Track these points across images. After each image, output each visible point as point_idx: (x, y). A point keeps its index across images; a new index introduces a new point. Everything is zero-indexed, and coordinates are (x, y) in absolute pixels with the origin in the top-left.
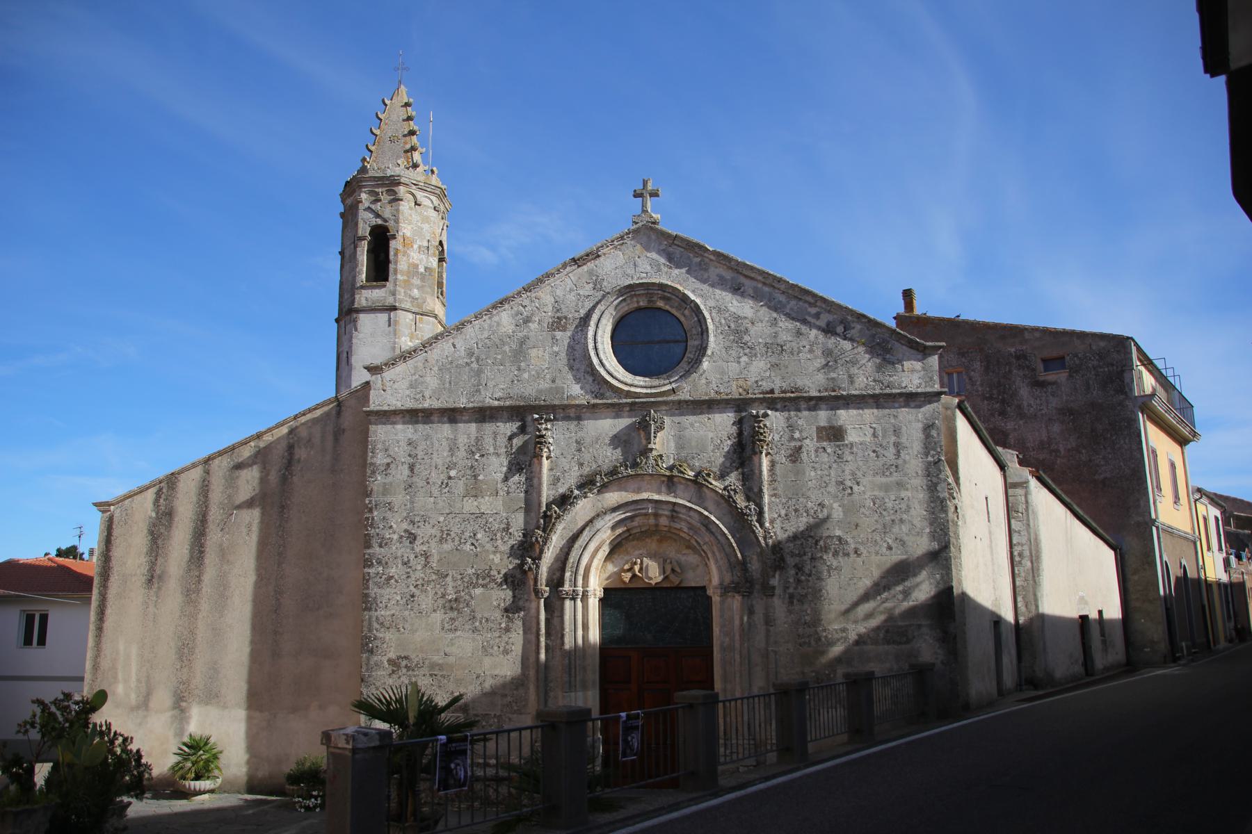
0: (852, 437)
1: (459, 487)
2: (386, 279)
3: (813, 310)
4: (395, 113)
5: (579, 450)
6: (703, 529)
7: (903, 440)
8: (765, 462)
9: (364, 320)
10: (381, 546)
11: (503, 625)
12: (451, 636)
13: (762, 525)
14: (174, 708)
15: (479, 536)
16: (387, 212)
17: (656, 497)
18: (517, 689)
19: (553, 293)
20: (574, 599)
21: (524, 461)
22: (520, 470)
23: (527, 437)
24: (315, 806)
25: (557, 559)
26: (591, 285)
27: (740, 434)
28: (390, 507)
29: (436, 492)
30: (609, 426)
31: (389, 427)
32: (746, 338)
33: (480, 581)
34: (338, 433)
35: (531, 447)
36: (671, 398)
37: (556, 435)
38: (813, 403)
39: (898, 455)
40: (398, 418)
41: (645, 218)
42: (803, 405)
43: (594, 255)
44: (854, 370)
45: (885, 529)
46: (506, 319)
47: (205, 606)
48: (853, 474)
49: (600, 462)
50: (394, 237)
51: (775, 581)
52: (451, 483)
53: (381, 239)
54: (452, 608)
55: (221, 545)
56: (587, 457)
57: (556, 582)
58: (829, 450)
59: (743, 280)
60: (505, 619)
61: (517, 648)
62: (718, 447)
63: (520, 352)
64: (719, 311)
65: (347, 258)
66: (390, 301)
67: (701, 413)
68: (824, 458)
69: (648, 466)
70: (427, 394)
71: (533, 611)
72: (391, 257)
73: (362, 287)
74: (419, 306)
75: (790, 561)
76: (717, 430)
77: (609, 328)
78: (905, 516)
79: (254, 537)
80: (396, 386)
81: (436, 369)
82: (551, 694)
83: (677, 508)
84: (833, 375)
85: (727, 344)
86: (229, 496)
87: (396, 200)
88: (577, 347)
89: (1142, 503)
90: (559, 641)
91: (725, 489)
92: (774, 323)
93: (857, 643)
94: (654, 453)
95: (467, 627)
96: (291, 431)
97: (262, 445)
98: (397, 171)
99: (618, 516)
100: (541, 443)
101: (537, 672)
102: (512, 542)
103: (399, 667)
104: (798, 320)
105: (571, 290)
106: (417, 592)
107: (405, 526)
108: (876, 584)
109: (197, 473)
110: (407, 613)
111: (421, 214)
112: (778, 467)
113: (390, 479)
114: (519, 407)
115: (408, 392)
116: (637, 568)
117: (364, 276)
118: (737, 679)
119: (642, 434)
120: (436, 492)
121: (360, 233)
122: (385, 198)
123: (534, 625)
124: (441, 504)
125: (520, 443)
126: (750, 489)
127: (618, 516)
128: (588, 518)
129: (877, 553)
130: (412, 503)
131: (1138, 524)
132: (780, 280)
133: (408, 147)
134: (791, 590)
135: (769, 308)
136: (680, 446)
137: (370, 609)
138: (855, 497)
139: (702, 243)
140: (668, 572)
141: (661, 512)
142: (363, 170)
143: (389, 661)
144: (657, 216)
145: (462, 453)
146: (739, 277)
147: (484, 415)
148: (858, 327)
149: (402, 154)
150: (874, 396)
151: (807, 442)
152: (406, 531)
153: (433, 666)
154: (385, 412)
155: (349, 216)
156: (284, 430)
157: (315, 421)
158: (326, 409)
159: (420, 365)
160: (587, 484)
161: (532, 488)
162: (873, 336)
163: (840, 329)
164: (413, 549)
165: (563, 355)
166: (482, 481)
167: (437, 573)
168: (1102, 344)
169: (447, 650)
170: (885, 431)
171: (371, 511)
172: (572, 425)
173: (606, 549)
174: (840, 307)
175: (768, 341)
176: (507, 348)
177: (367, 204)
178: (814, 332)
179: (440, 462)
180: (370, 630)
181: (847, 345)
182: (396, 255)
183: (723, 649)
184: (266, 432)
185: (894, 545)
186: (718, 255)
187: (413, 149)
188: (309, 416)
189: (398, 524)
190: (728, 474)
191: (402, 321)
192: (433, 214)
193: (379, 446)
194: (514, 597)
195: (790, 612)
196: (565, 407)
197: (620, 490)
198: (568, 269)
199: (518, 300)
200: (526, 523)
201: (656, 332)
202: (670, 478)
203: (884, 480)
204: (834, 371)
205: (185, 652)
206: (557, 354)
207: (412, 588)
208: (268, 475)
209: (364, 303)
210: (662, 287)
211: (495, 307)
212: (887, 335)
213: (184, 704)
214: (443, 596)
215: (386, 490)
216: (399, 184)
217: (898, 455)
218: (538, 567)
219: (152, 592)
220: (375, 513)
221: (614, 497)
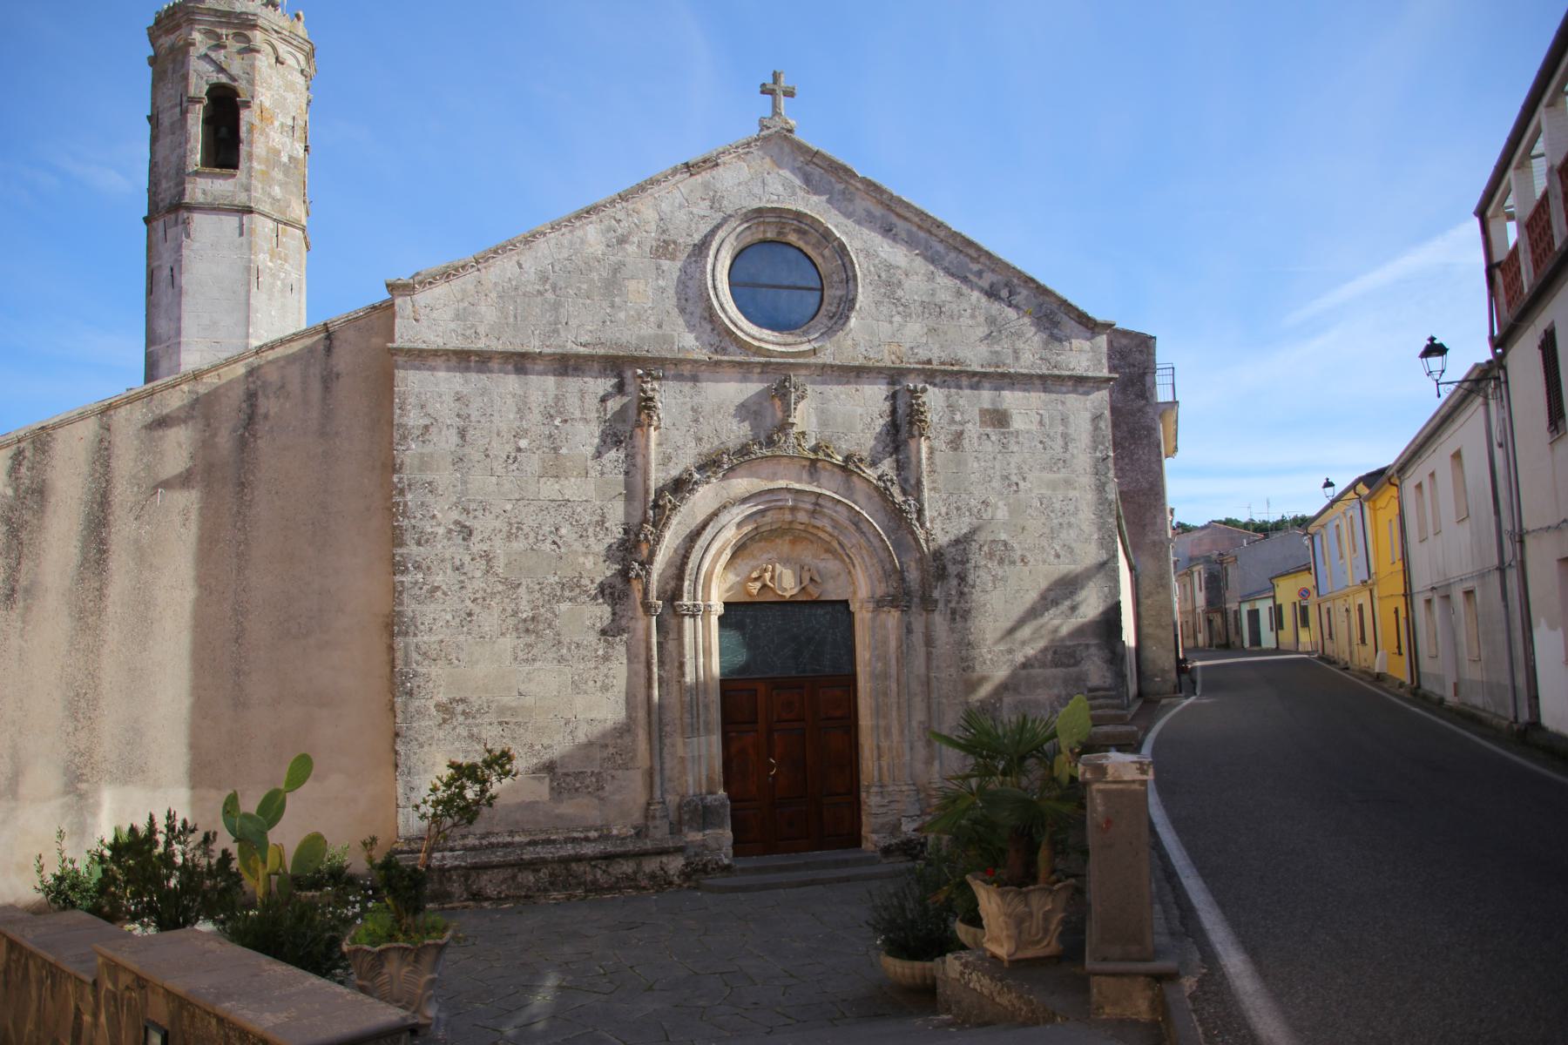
0: (1017, 423)
1: (533, 463)
2: (236, 167)
3: (975, 267)
5: (696, 421)
6: (852, 528)
7: (1071, 431)
8: (924, 445)
10: (419, 544)
11: (600, 652)
12: (527, 668)
13: (922, 525)
14: (66, 793)
15: (563, 531)
16: (236, 66)
17: (797, 486)
18: (621, 737)
19: (656, 207)
20: (694, 616)
21: (623, 431)
22: (618, 443)
23: (626, 399)
24: (356, 916)
25: (669, 564)
26: (708, 203)
27: (894, 412)
28: (431, 487)
29: (499, 470)
30: (733, 391)
32: (900, 293)
33: (567, 593)
34: (329, 380)
35: (632, 412)
36: (812, 360)
37: (668, 398)
38: (976, 379)
39: (1066, 447)
40: (439, 361)
41: (777, 125)
42: (965, 381)
43: (711, 163)
44: (1020, 344)
45: (1053, 534)
46: (592, 235)
47: (113, 634)
48: (1019, 468)
49: (724, 438)
50: (247, 105)
51: (936, 594)
52: (521, 457)
53: (225, 109)
54: (527, 630)
55: (137, 541)
56: (706, 430)
57: (672, 596)
58: (993, 438)
59: (894, 219)
60: (602, 644)
61: (620, 683)
62: (868, 426)
63: (613, 283)
64: (868, 255)
66: (241, 199)
67: (848, 383)
68: (988, 446)
69: (788, 445)
70: (482, 330)
71: (641, 633)
73: (197, 173)
74: (284, 213)
75: (953, 569)
76: (871, 401)
77: (728, 263)
78: (1073, 520)
79: (193, 528)
80: (435, 315)
81: (494, 295)
82: (668, 741)
83: (821, 501)
84: (997, 348)
85: (878, 298)
86: (148, 467)
88: (690, 283)
89: (1159, 521)
90: (676, 672)
91: (880, 478)
92: (931, 277)
93: (1024, 666)
94: (795, 430)
95: (550, 655)
96: (251, 372)
97: (202, 390)
99: (748, 509)
100: (649, 408)
101: (649, 713)
102: (609, 540)
103: (453, 714)
104: (958, 277)
105: (681, 206)
106: (476, 609)
107: (455, 515)
108: (1043, 597)
109: (89, 429)
110: (462, 638)
112: (937, 453)
113: (428, 449)
114: (617, 357)
115: (453, 325)
116: (768, 576)
118: (894, 714)
119: (778, 403)
120: (499, 470)
121: (192, 92)
122: (233, 45)
123: (643, 651)
124: (507, 486)
125: (617, 407)
126: (906, 480)
127: (748, 509)
128: (710, 511)
129: (1044, 562)
130: (465, 483)
131: (1154, 544)
132: (940, 225)
134: (953, 605)
135: (926, 258)
136: (823, 423)
137: (406, 634)
138: (1021, 495)
139: (849, 165)
140: (806, 582)
141: (801, 505)
143: (437, 706)
144: (793, 122)
145: (536, 416)
146: (894, 216)
147: (566, 365)
148: (1025, 292)
150: (1042, 377)
151: (970, 426)
152: (457, 523)
153: (502, 710)
154: (421, 351)
155: (167, 64)
156: (240, 369)
157: (291, 359)
158: (308, 342)
159: (471, 287)
160: (710, 465)
161: (633, 469)
162: (1041, 306)
163: (1004, 293)
164: (468, 548)
165: (671, 292)
166: (565, 456)
167: (505, 581)
168: (1124, 341)
169: (522, 688)
170: (1052, 419)
171: (402, 492)
172: (687, 387)
173: (728, 554)
174: (1007, 266)
175: (925, 298)
176: (595, 276)
177: (203, 50)
178: (976, 294)
179: (504, 427)
180: (407, 664)
181: (1011, 313)
183: (874, 676)
184: (208, 371)
185: (1062, 553)
186: (865, 181)
188: (280, 352)
189: (444, 514)
190: (881, 460)
192: (301, 80)
193: (412, 400)
194: (614, 614)
195: (952, 630)
196: (677, 362)
197: (751, 475)
198: (678, 177)
199: (610, 211)
200: (627, 514)
201: (789, 271)
202: (814, 462)
203: (1052, 476)
204: (998, 342)
205: (81, 704)
206: (663, 290)
207: (468, 603)
208: (214, 435)
209: (200, 198)
210: (799, 216)
211: (578, 217)
212: (1054, 307)
213: (84, 786)
214: (515, 613)
215: (424, 463)
216: (254, 26)
217: (1066, 447)
218: (648, 573)
219: (13, 615)
220: (409, 497)
221: (742, 484)
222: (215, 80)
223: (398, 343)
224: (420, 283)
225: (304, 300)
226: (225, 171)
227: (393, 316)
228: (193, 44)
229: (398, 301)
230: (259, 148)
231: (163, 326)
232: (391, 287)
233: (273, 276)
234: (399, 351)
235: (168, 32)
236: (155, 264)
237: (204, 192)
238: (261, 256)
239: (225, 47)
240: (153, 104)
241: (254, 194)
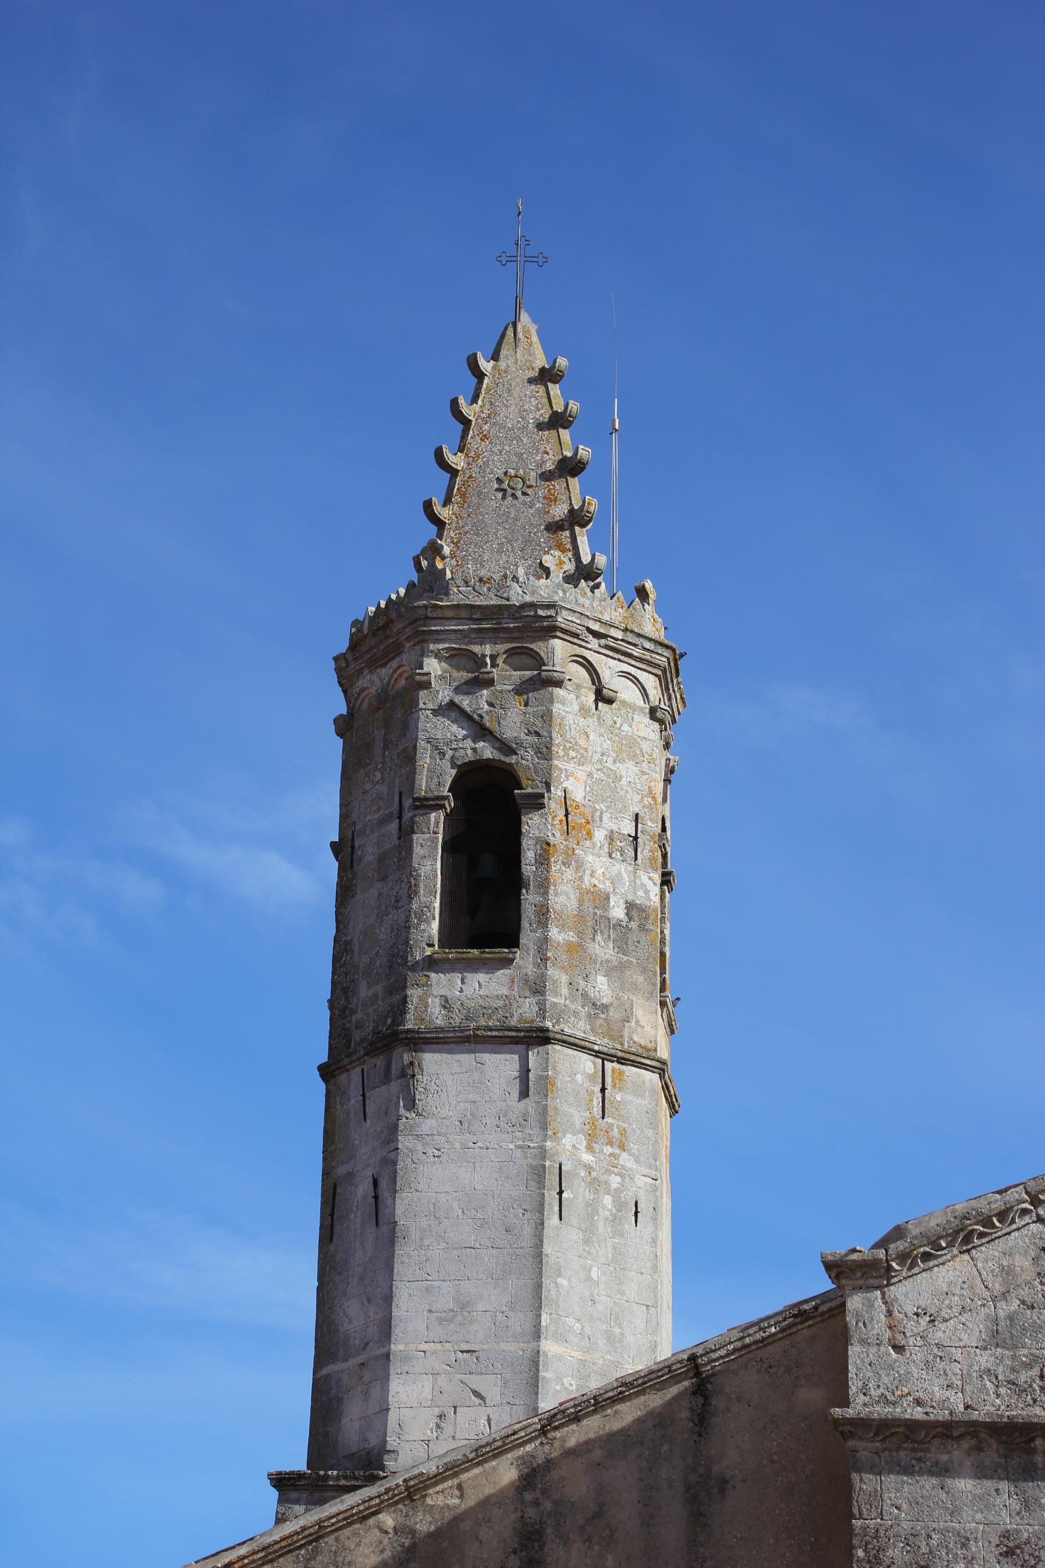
2: (512, 941)
9: (441, 1074)
16: (512, 723)
31: (928, 1483)
40: (957, 1453)
50: (537, 803)
53: (493, 811)
65: (364, 863)
66: (525, 1010)
72: (528, 868)
73: (431, 964)
80: (940, 1334)
87: (542, 681)
96: (532, 1477)
97: (423, 1524)
98: (544, 590)
111: (612, 729)
115: (985, 1359)
117: (435, 925)
121: (423, 784)
122: (507, 677)
133: (560, 511)
142: (430, 581)
149: (543, 537)
154: (912, 1425)
155: (373, 733)
156: (506, 1472)
157: (616, 1444)
158: (655, 1400)
177: (444, 694)
182: (543, 859)
184: (438, 1478)
187: (577, 518)
188: (593, 1426)
191: (562, 1080)
192: (650, 730)
209: (437, 1016)
216: (551, 631)
222: (470, 756)
223: (858, 1407)
224: (902, 1257)
225: (665, 1234)
226: (489, 953)
227: (843, 1337)
228: (427, 685)
229: (855, 1302)
230: (563, 896)
231: (354, 1317)
232: (835, 1268)
233: (596, 1185)
234: (862, 1424)
235: (376, 662)
236: (341, 1170)
237: (446, 1004)
238: (568, 1140)
239: (490, 683)
240: (344, 817)
241: (551, 999)
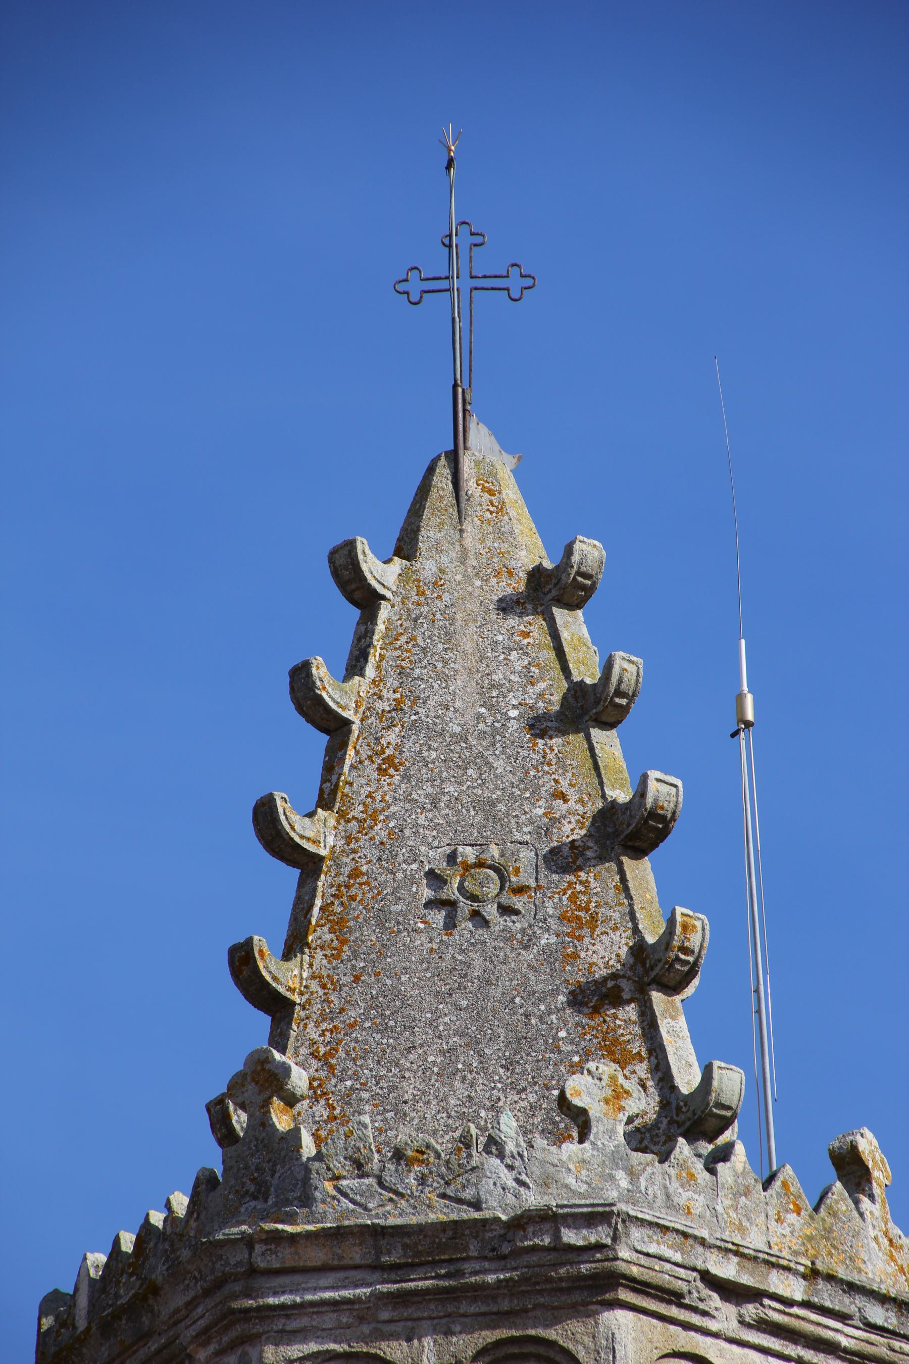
4: (461, 662)
98: (576, 1172)
133: (606, 952)
142: (256, 1167)
149: (566, 1026)
187: (655, 969)
